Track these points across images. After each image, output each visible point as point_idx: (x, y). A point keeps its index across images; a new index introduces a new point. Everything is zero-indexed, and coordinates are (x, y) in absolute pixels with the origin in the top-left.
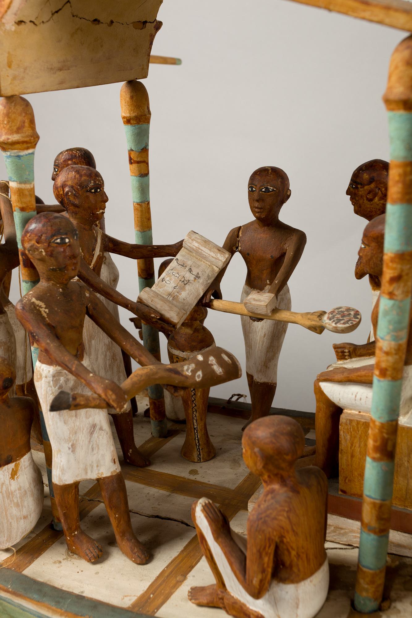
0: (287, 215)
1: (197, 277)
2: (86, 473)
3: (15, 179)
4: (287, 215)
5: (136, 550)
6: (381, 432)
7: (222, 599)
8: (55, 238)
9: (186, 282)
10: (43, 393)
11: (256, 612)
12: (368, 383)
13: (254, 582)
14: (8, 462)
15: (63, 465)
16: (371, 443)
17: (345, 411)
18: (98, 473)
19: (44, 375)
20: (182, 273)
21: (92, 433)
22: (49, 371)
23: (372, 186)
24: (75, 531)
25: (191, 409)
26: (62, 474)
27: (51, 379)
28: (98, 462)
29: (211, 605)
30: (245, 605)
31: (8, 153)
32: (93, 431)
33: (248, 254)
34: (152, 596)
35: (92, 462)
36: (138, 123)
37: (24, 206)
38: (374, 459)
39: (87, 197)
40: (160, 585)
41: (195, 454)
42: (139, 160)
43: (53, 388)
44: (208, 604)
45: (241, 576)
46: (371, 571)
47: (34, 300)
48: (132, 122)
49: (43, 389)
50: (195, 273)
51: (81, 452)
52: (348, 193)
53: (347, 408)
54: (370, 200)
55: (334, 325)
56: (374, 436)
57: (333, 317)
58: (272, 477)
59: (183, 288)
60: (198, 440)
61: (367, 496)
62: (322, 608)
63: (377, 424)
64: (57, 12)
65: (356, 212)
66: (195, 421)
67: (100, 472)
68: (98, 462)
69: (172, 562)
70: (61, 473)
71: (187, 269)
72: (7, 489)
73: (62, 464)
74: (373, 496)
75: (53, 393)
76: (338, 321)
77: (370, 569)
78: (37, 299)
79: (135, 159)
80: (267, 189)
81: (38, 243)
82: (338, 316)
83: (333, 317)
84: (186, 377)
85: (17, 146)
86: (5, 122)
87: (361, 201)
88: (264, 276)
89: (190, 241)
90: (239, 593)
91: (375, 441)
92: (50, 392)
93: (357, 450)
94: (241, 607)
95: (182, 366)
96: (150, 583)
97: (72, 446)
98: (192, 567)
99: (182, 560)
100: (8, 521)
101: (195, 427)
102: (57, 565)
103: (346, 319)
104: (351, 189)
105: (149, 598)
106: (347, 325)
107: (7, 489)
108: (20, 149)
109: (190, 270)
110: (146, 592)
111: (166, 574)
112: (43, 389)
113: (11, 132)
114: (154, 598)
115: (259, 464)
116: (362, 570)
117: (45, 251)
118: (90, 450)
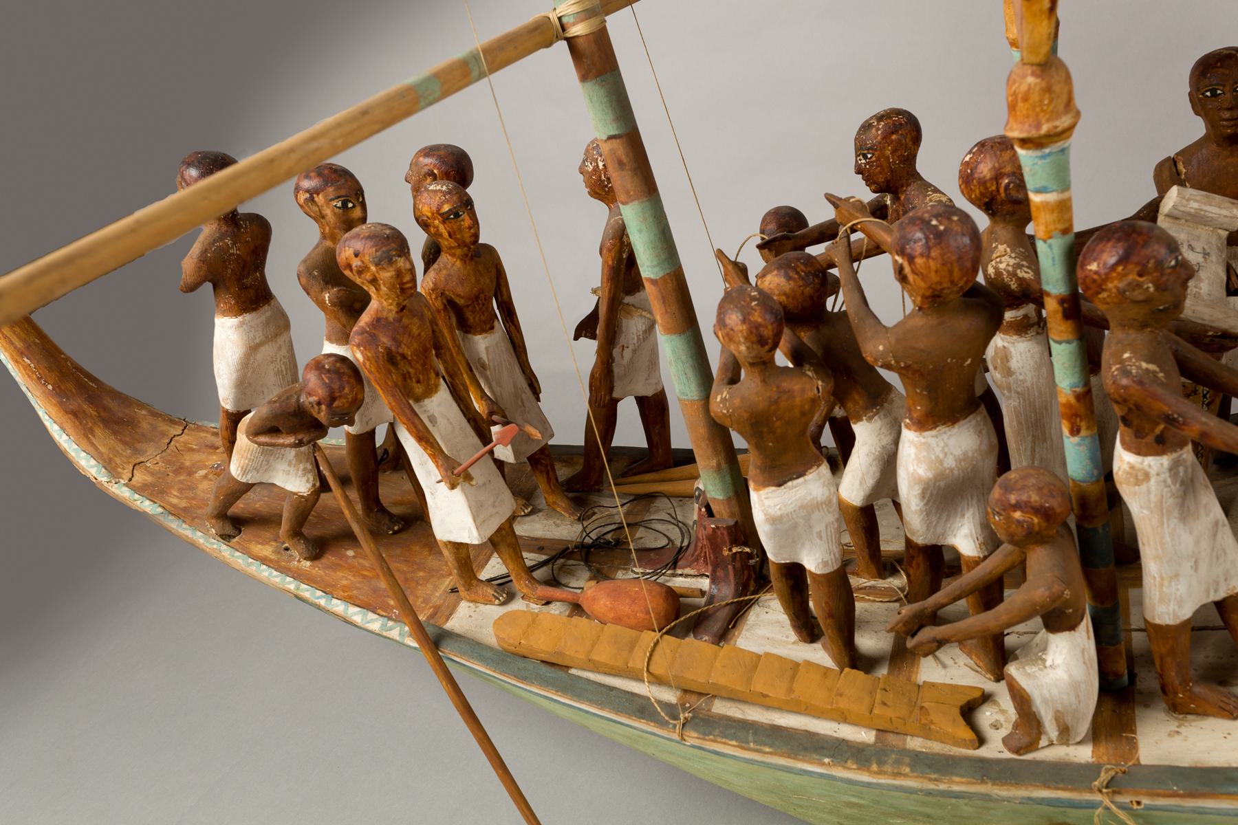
1: (1206, 255)
3: (1055, 187)
21: (1215, 535)
31: (1047, 151)
47: (1144, 365)
51: (1203, 567)
78: (1148, 362)
81: (1140, 275)
89: (1185, 202)
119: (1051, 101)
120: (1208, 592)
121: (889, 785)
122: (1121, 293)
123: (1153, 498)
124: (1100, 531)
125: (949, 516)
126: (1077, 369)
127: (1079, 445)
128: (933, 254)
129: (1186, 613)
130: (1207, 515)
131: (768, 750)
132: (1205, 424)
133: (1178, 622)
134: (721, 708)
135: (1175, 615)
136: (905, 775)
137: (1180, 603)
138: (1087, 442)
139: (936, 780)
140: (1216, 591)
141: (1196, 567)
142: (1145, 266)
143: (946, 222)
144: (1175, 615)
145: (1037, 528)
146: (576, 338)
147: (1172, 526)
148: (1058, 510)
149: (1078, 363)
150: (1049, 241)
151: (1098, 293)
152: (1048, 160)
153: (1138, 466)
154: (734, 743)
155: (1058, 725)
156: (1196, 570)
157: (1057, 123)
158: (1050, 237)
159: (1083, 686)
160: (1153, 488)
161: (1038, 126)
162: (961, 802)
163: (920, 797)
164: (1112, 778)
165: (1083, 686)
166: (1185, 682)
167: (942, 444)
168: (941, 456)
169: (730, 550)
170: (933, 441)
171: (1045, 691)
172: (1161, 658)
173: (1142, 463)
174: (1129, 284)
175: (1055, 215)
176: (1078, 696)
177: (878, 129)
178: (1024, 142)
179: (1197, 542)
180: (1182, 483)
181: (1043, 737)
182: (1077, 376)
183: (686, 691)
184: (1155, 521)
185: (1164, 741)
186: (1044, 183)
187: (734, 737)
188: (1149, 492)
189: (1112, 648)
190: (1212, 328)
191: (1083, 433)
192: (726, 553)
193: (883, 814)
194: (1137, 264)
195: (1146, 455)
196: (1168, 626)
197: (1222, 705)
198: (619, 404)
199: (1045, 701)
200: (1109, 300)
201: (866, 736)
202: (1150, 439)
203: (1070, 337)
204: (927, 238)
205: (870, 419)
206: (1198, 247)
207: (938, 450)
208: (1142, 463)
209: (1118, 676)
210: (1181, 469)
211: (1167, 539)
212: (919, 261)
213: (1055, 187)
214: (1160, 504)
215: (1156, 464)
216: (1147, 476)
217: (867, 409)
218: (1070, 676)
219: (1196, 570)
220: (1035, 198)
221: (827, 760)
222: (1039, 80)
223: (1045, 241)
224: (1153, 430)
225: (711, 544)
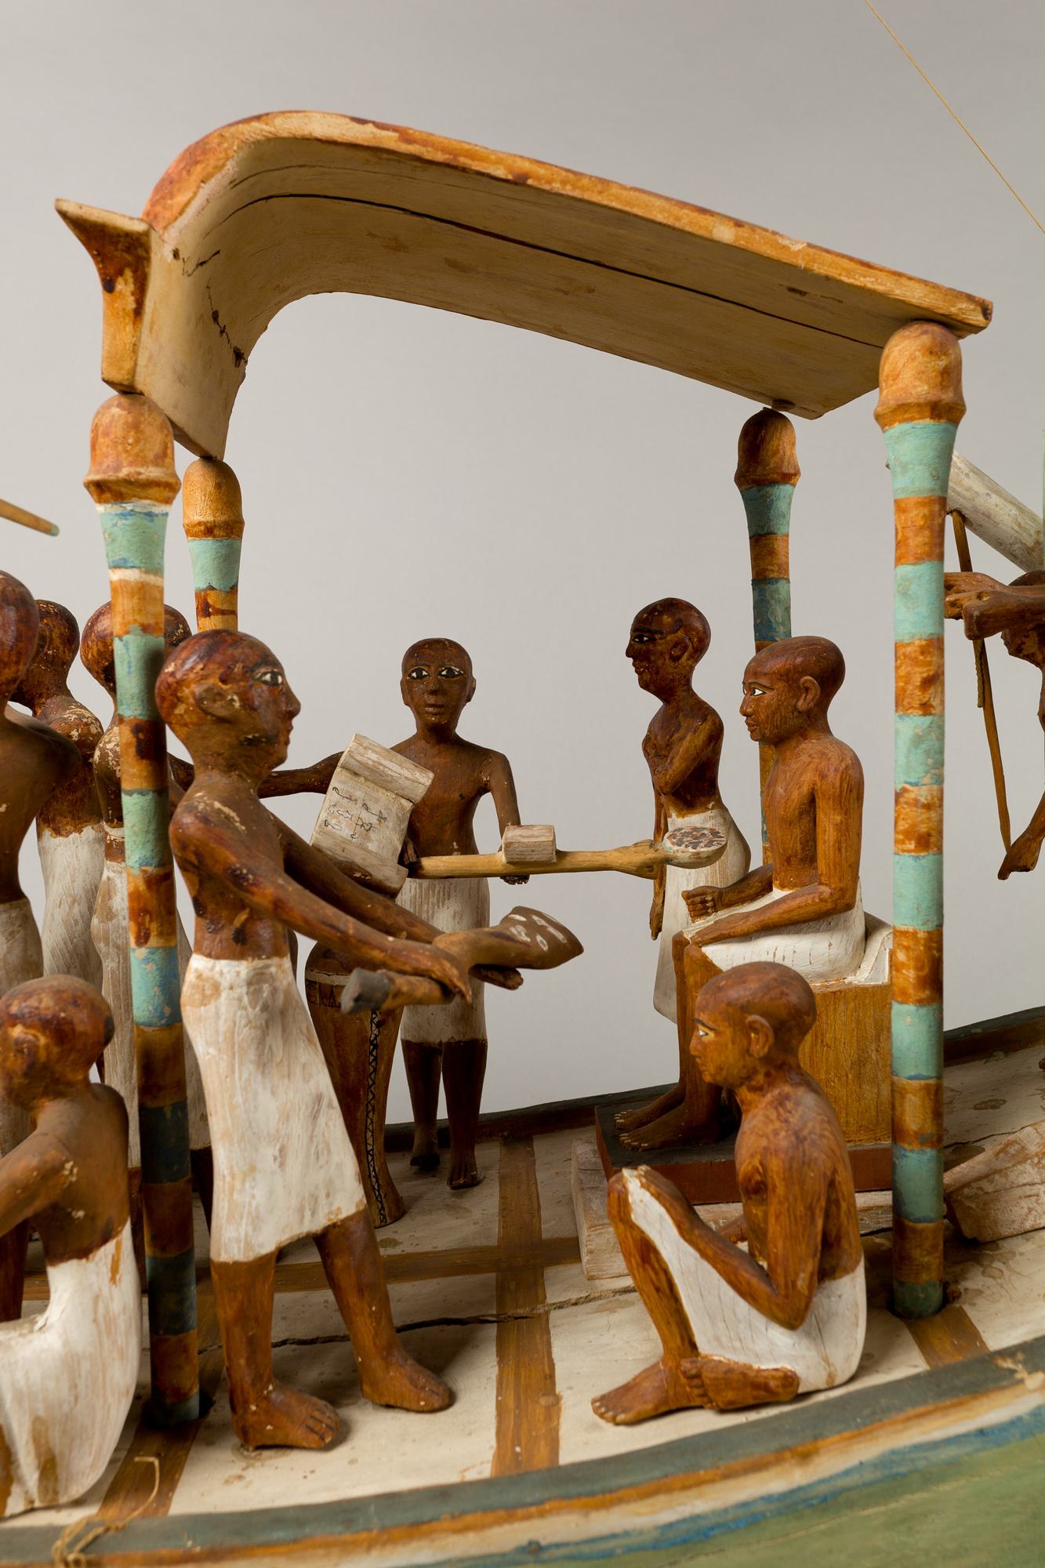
0: (470, 726)
1: (382, 818)
3: (137, 563)
4: (470, 726)
5: (422, 1381)
7: (698, 1376)
8: (263, 670)
11: (776, 1370)
13: (799, 1283)
14: (105, 1240)
15: (257, 1208)
18: (330, 1213)
19: (225, 984)
21: (315, 1117)
22: (238, 973)
23: (680, 634)
24: (269, 1381)
25: (362, 1108)
26: (254, 1230)
27: (244, 990)
28: (330, 1183)
29: (663, 1409)
30: (750, 1368)
31: (129, 507)
32: (318, 1111)
34: (518, 1449)
35: (317, 1188)
36: (228, 536)
37: (151, 621)
42: (225, 607)
43: (250, 1009)
44: (656, 1408)
46: (931, 1225)
47: (217, 805)
48: (216, 532)
49: (223, 1018)
50: (375, 808)
51: (294, 1166)
52: (628, 654)
54: (676, 659)
55: (690, 850)
58: (773, 1072)
60: (376, 1177)
61: (911, 1078)
63: (921, 935)
64: (202, 264)
65: (645, 685)
66: (369, 1134)
67: (334, 1208)
68: (330, 1183)
70: (250, 1229)
72: (107, 1308)
73: (254, 1203)
74: (924, 1073)
75: (250, 1022)
77: (931, 1221)
78: (224, 803)
79: (218, 606)
80: (450, 670)
81: (224, 681)
85: (154, 491)
86: (130, 441)
87: (660, 662)
88: (447, 836)
89: (362, 750)
90: (737, 1344)
92: (243, 1022)
94: (744, 1375)
96: (493, 1431)
97: (281, 1151)
98: (551, 1377)
99: (517, 1376)
100: (105, 1402)
101: (370, 1148)
102: (238, 1484)
104: (637, 646)
105: (518, 1454)
107: (107, 1308)
108: (156, 500)
109: (366, 807)
110: (499, 1447)
111: (511, 1404)
112: (223, 1018)
113: (140, 459)
116: (914, 1231)
117: (241, 700)
118: (313, 1158)
119: (137, 441)
120: (301, 1211)
122: (199, 701)
123: (223, 1027)
124: (169, 1115)
126: (151, 837)
127: (147, 960)
129: (267, 1242)
130: (306, 1081)
132: (282, 887)
133: (251, 1256)
135: (248, 1245)
137: (256, 1221)
138: (157, 957)
140: (313, 1213)
141: (282, 1157)
144: (248, 1245)
145: (42, 1056)
147: (245, 1076)
148: (80, 1028)
149: (153, 827)
150: (125, 637)
151: (174, 706)
152: (130, 521)
153: (206, 974)
155: (38, 1455)
156: (282, 1165)
157: (142, 470)
158: (127, 632)
159: (86, 1366)
160: (223, 1009)
161: (118, 469)
164: (96, 1538)
165: (86, 1366)
166: (259, 1380)
171: (19, 1375)
172: (228, 1331)
173: (212, 969)
174: (208, 690)
175: (135, 600)
176: (74, 1386)
179: (286, 1118)
180: (265, 1008)
181: (15, 1489)
182: (149, 846)
184: (223, 1065)
185: (218, 1485)
186: (124, 554)
188: (217, 1014)
189: (173, 1338)
191: (153, 941)
194: (221, 664)
195: (218, 957)
196: (236, 1263)
197: (311, 1423)
199: (19, 1397)
200: (187, 718)
202: (227, 933)
203: (145, 786)
206: (375, 808)
208: (212, 969)
209: (181, 1396)
210: (266, 987)
211: (239, 1099)
213: (137, 563)
214: (231, 1034)
215: (232, 972)
216: (216, 988)
218: (66, 1343)
219: (282, 1165)
222: (124, 413)
223: (121, 639)
224: (231, 921)
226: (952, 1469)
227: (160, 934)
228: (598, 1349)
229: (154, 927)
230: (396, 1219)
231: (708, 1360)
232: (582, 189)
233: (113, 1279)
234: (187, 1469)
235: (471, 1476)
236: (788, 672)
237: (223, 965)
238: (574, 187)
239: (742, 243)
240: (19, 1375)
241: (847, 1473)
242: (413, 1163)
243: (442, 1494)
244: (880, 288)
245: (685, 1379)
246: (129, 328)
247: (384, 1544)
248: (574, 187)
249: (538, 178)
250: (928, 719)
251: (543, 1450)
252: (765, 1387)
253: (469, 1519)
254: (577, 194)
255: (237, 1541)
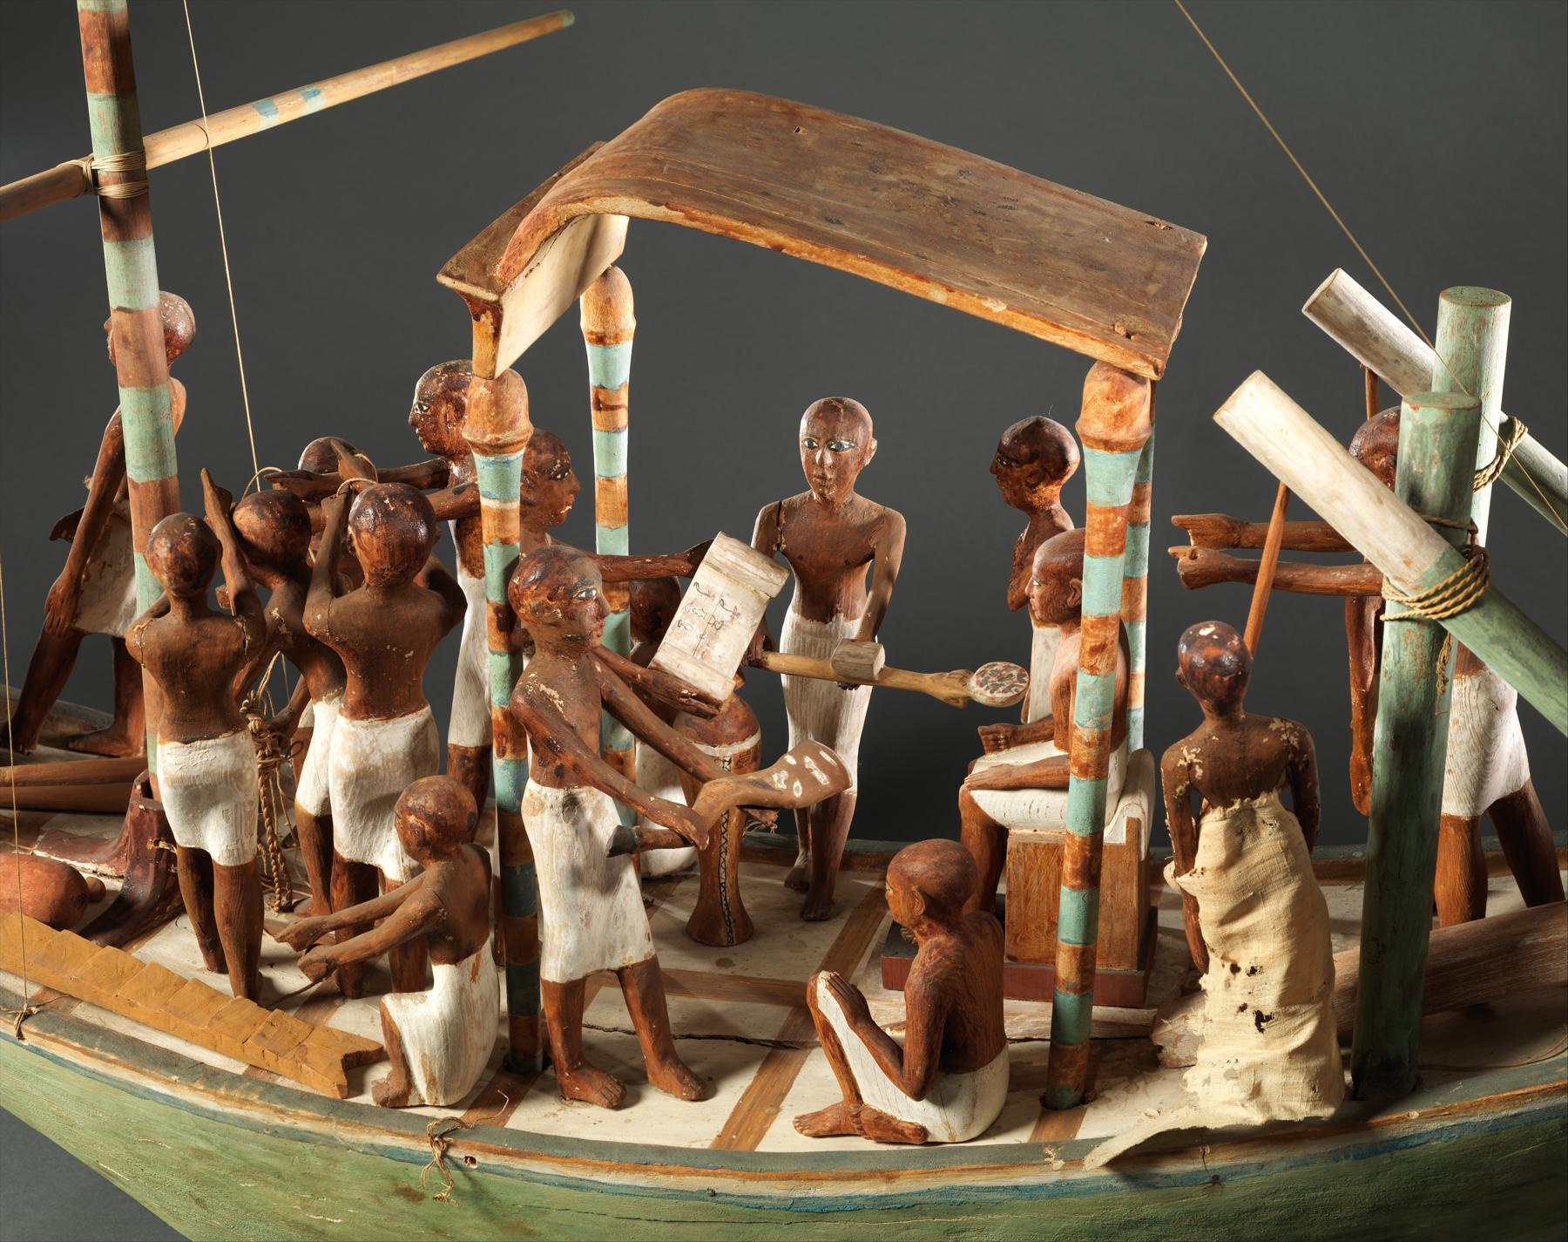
1: (735, 614)
2: (603, 960)
6: (1082, 850)
9: (718, 626)
10: (546, 833)
12: (1063, 787)
14: (468, 954)
16: (1068, 866)
17: (1012, 831)
20: (710, 610)
33: (801, 557)
38: (1073, 888)
39: (551, 488)
40: (742, 1122)
41: (723, 933)
45: (894, 1071)
47: (543, 687)
50: (730, 606)
53: (1015, 826)
55: (988, 694)
56: (1073, 856)
57: (986, 681)
59: (714, 637)
62: (1006, 1104)
69: (747, 1092)
71: (717, 599)
76: (995, 688)
82: (993, 679)
83: (986, 681)
84: (780, 791)
91: (1074, 863)
93: (1035, 888)
95: (770, 775)
98: (783, 1096)
102: (552, 1119)
103: (1007, 683)
106: (1009, 694)
114: (740, 1140)
115: (917, 908)
119: (497, 414)
121: (236, 1117)
125: (375, 826)
128: (378, 532)
131: (113, 1057)
134: (81, 1012)
136: (252, 1103)
138: (511, 766)
139: (282, 1112)
142: (556, 591)
143: (398, 503)
146: (53, 538)
154: (77, 1045)
156: (587, 925)
162: (308, 1147)
163: (265, 1138)
167: (371, 738)
168: (368, 750)
169: (157, 843)
170: (363, 732)
177: (439, 381)
178: (486, 450)
183: (47, 989)
187: (80, 1039)
190: (689, 686)
191: (508, 756)
192: (150, 846)
193: (234, 1171)
194: (548, 587)
198: (84, 639)
201: (239, 1068)
202: (551, 768)
203: (502, 649)
204: (376, 515)
205: (330, 700)
206: (730, 606)
207: (366, 743)
212: (365, 536)
217: (329, 687)
220: (484, 502)
221: (175, 1078)
225: (136, 830)
226: (995, 1206)
227: (514, 751)
228: (814, 1084)
229: (509, 746)
230: (742, 941)
231: (868, 1108)
232: (825, 258)
233: (473, 979)
234: (1357, 969)
235: (696, 1146)
236: (1060, 572)
237: (547, 790)
238: (819, 257)
239: (953, 304)
240: (414, 1027)
241: (920, 1193)
242: (787, 884)
243: (662, 1151)
244: (1068, 345)
245: (854, 1117)
246: (491, 344)
247: (619, 1171)
248: (819, 257)
249: (791, 249)
250: (1094, 678)
251: (750, 1141)
252: (902, 1133)
253: (671, 1168)
254: (821, 261)
255: (533, 1150)
